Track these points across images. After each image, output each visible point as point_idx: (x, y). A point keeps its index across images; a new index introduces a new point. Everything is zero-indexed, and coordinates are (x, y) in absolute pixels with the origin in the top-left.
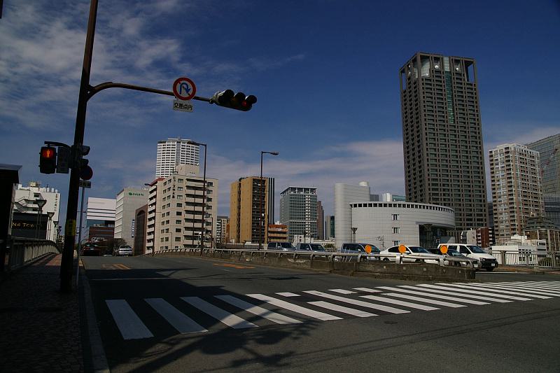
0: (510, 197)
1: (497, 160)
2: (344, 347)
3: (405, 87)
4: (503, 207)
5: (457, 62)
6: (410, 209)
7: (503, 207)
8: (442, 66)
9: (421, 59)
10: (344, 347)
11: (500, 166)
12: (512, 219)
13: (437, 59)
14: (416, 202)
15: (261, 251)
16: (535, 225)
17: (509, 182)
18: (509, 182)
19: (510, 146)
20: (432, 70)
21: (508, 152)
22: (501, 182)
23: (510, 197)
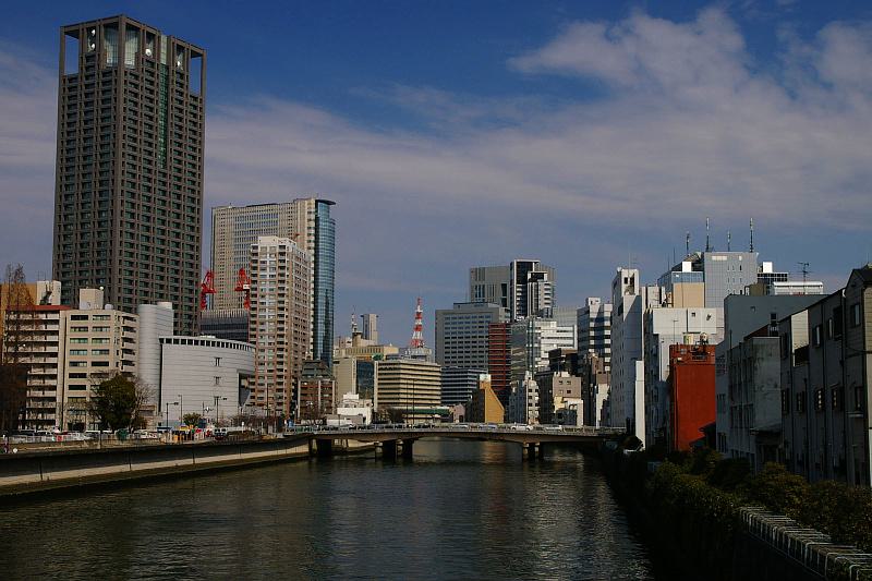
0: (279, 326)
1: (264, 262)
2: (845, 436)
3: (72, 69)
4: (266, 340)
5: (180, 49)
6: (180, 346)
7: (266, 340)
8: (156, 51)
9: (127, 28)
10: (845, 436)
11: (268, 273)
12: (279, 360)
13: (151, 37)
14: (190, 334)
15: (480, 427)
16: (315, 372)
17: (279, 302)
18: (279, 302)
19: (287, 244)
20: (139, 55)
21: (282, 254)
22: (267, 300)
23: (279, 326)
